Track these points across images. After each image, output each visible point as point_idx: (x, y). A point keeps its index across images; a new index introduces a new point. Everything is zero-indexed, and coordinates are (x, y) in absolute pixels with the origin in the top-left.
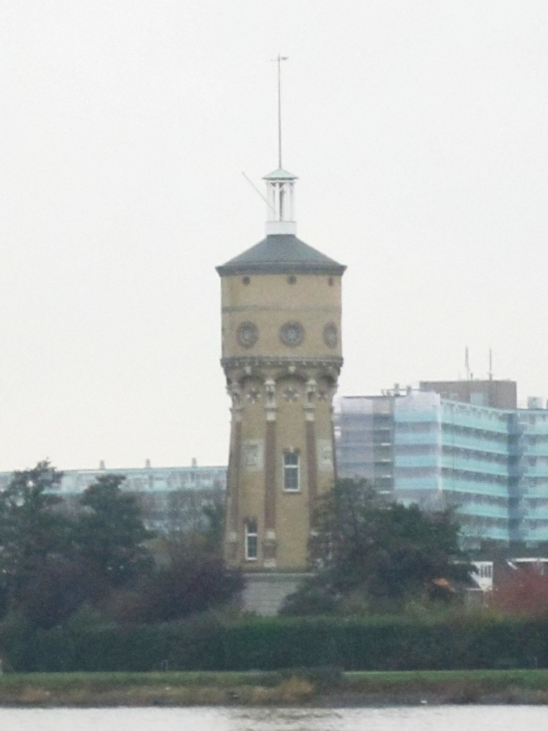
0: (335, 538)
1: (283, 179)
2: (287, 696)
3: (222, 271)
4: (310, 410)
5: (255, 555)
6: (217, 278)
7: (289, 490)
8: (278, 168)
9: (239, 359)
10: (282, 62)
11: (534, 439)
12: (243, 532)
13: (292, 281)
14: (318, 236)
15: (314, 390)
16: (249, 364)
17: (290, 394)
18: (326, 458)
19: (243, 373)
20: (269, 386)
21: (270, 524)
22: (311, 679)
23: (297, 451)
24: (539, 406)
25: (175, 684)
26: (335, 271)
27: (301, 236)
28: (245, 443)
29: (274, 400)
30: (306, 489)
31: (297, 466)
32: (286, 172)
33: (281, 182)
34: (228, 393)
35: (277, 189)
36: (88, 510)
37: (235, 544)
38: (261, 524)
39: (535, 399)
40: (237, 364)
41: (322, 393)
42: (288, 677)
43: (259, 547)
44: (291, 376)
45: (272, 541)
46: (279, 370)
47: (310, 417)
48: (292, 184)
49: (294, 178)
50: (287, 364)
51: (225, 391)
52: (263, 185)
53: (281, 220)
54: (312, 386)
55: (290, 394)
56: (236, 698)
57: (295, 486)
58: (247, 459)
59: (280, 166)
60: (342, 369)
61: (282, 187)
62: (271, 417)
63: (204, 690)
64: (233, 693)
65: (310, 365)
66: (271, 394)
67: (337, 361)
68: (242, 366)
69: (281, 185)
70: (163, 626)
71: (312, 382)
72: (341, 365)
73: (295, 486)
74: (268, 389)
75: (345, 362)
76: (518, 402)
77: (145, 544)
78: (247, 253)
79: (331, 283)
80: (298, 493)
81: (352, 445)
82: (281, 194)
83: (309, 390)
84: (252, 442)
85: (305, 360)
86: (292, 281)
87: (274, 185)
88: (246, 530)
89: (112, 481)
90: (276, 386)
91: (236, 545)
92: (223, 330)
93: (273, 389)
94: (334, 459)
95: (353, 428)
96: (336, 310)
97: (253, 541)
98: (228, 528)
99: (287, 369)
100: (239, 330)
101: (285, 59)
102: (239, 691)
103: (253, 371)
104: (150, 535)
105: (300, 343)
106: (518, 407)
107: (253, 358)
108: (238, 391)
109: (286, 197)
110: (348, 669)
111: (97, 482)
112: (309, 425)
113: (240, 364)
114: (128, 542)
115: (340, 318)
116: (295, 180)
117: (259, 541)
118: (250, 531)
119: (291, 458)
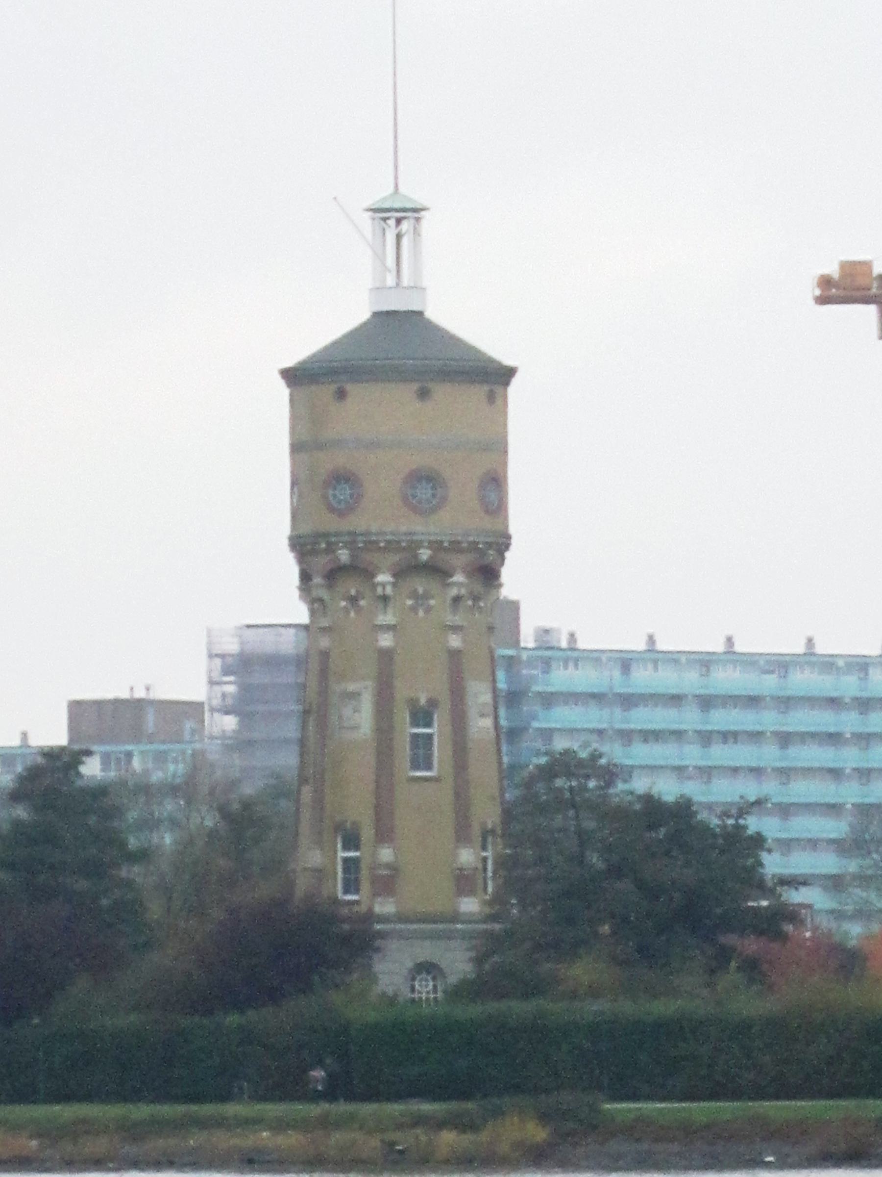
2: (504, 1148)
3: (294, 377)
5: (357, 891)
7: (418, 774)
8: (391, 190)
9: (326, 535)
11: (549, 700)
12: (335, 852)
13: (423, 394)
14: (462, 312)
15: (463, 591)
16: (345, 547)
17: (420, 599)
18: (482, 715)
19: (328, 558)
20: (384, 585)
21: (385, 833)
22: (544, 1117)
23: (433, 703)
24: (555, 644)
25: (280, 1126)
26: (495, 377)
27: (432, 314)
28: (336, 688)
29: (390, 611)
32: (410, 200)
33: (398, 216)
34: (301, 597)
36: (21, 812)
37: (319, 871)
38: (367, 834)
39: (547, 631)
40: (323, 546)
41: (476, 599)
42: (498, 1113)
43: (364, 873)
44: (422, 568)
45: (388, 866)
47: (455, 641)
48: (418, 219)
49: (422, 210)
50: (414, 546)
51: (296, 593)
52: (366, 221)
53: (398, 285)
54: (460, 585)
55: (420, 599)
56: (401, 1152)
58: (340, 717)
60: (507, 555)
61: (400, 228)
62: (386, 641)
63: (337, 1137)
64: (392, 1144)
65: (455, 547)
66: (385, 599)
67: (501, 540)
68: (331, 549)
69: (399, 221)
70: (233, 1019)
71: (459, 578)
72: (507, 546)
74: (379, 590)
75: (514, 541)
76: (522, 637)
77: (134, 872)
79: (491, 398)
80: (436, 779)
81: (261, 708)
82: (399, 237)
83: (454, 592)
84: (351, 687)
85: (448, 538)
86: (423, 394)
87: (384, 220)
88: (339, 846)
89: (66, 759)
90: (394, 585)
91: (320, 873)
92: (294, 484)
93: (389, 590)
94: (496, 718)
95: (260, 678)
96: (498, 447)
97: (350, 865)
98: (304, 841)
99: (416, 556)
100: (325, 482)
102: (404, 1140)
103: (353, 556)
104: (143, 856)
105: (434, 510)
106: (522, 645)
107: (352, 534)
108: (324, 594)
109: (405, 241)
110: (617, 1097)
111: (40, 760)
112: (455, 655)
113: (329, 544)
114: (96, 870)
115: (505, 464)
116: (423, 213)
117: (363, 865)
118: (346, 848)
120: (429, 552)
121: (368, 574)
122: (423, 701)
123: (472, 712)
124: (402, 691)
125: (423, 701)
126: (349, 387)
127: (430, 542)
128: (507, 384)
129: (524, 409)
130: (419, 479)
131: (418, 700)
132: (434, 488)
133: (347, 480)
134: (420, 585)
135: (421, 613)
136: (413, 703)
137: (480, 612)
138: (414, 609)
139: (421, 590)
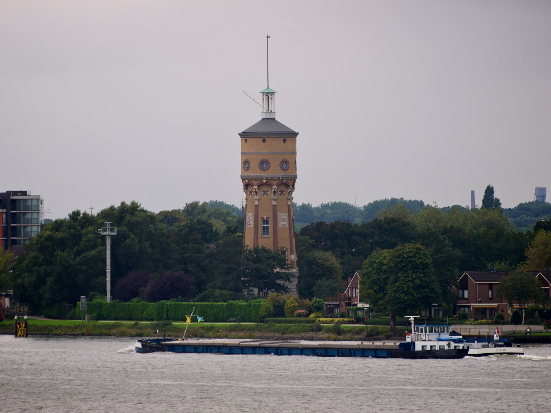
3: (245, 135)
4: (274, 200)
13: (264, 141)
14: (286, 119)
23: (268, 218)
26: (294, 135)
30: (272, 235)
33: (269, 95)
35: (265, 97)
46: (258, 182)
47: (274, 203)
50: (261, 179)
55: (282, 192)
62: (257, 203)
65: (272, 179)
66: (256, 192)
86: (264, 141)
90: (277, 189)
103: (248, 181)
112: (274, 206)
119: (266, 222)
122: (265, 218)
123: (253, 219)
124: (260, 216)
125: (265, 218)
129: (301, 145)
130: (263, 162)
133: (266, 162)
134: (283, 188)
136: (263, 218)
138: (263, 195)
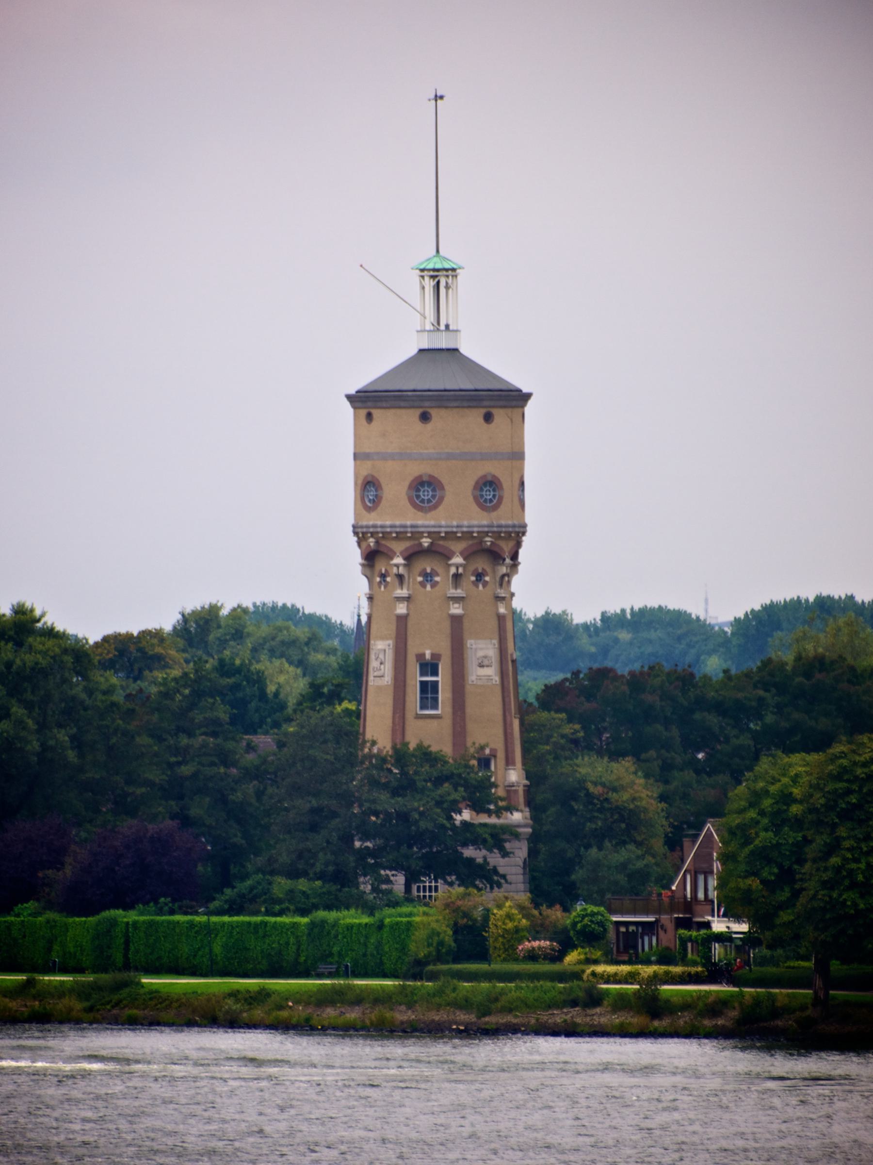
0: (762, 813)
1: (438, 270)
3: (366, 401)
6: (348, 410)
10: (439, 101)
13: (425, 417)
20: (397, 566)
23: (436, 657)
30: (449, 709)
31: (420, 679)
32: (445, 259)
33: (440, 277)
35: (429, 284)
47: (456, 609)
50: (417, 535)
55: (428, 577)
57: (435, 706)
59: (438, 251)
65: (451, 535)
66: (400, 577)
67: (522, 530)
72: (524, 533)
73: (435, 706)
78: (367, 385)
86: (425, 417)
90: (465, 567)
93: (402, 570)
101: (442, 97)
112: (456, 620)
119: (430, 667)
120: (429, 540)
121: (446, 556)
122: (428, 656)
125: (428, 656)
126: (433, 412)
127: (429, 533)
128: (523, 406)
130: (485, 484)
131: (424, 655)
132: (434, 490)
134: (481, 564)
135: (428, 588)
136: (420, 657)
137: (484, 586)
139: (429, 570)
